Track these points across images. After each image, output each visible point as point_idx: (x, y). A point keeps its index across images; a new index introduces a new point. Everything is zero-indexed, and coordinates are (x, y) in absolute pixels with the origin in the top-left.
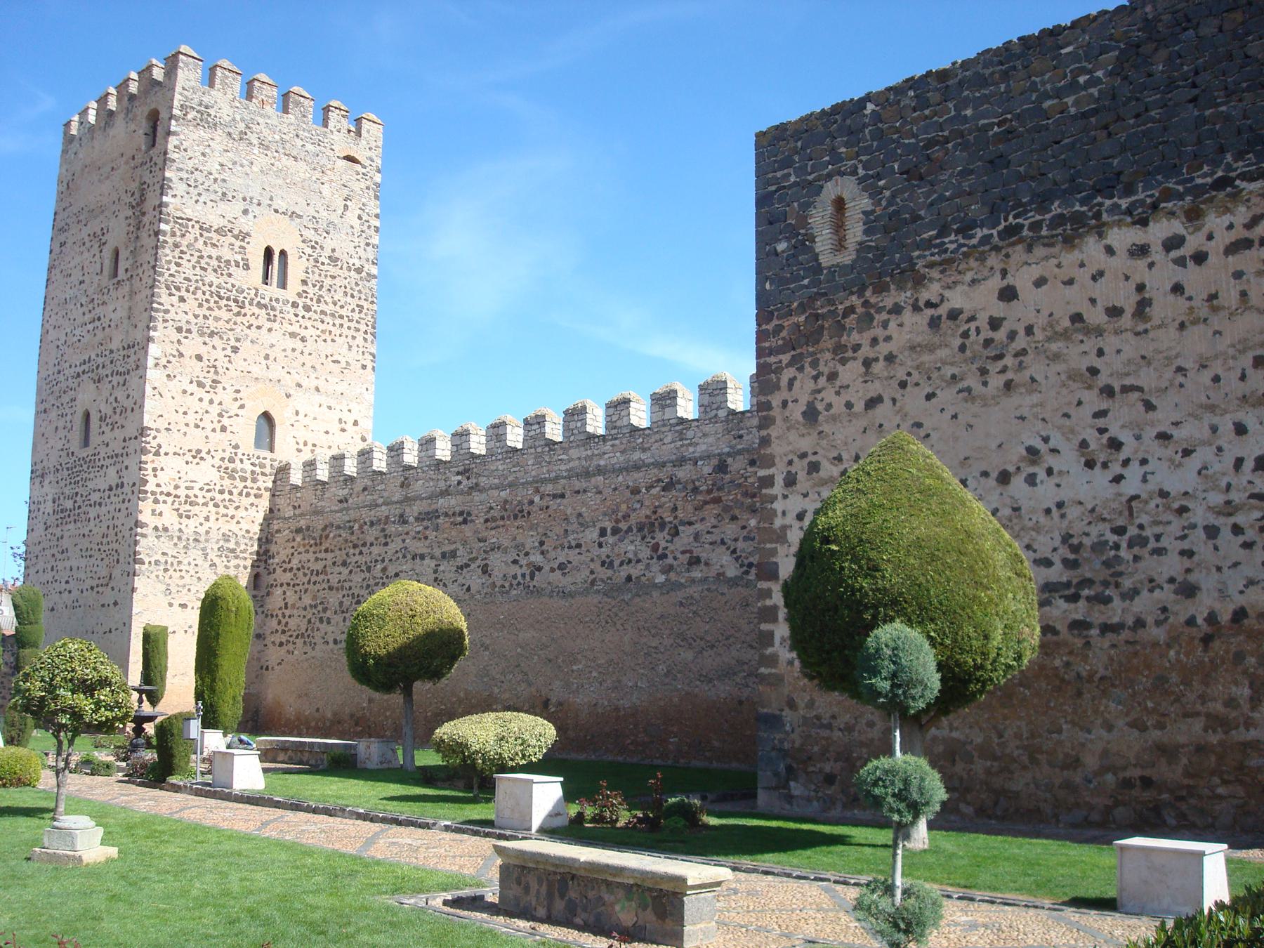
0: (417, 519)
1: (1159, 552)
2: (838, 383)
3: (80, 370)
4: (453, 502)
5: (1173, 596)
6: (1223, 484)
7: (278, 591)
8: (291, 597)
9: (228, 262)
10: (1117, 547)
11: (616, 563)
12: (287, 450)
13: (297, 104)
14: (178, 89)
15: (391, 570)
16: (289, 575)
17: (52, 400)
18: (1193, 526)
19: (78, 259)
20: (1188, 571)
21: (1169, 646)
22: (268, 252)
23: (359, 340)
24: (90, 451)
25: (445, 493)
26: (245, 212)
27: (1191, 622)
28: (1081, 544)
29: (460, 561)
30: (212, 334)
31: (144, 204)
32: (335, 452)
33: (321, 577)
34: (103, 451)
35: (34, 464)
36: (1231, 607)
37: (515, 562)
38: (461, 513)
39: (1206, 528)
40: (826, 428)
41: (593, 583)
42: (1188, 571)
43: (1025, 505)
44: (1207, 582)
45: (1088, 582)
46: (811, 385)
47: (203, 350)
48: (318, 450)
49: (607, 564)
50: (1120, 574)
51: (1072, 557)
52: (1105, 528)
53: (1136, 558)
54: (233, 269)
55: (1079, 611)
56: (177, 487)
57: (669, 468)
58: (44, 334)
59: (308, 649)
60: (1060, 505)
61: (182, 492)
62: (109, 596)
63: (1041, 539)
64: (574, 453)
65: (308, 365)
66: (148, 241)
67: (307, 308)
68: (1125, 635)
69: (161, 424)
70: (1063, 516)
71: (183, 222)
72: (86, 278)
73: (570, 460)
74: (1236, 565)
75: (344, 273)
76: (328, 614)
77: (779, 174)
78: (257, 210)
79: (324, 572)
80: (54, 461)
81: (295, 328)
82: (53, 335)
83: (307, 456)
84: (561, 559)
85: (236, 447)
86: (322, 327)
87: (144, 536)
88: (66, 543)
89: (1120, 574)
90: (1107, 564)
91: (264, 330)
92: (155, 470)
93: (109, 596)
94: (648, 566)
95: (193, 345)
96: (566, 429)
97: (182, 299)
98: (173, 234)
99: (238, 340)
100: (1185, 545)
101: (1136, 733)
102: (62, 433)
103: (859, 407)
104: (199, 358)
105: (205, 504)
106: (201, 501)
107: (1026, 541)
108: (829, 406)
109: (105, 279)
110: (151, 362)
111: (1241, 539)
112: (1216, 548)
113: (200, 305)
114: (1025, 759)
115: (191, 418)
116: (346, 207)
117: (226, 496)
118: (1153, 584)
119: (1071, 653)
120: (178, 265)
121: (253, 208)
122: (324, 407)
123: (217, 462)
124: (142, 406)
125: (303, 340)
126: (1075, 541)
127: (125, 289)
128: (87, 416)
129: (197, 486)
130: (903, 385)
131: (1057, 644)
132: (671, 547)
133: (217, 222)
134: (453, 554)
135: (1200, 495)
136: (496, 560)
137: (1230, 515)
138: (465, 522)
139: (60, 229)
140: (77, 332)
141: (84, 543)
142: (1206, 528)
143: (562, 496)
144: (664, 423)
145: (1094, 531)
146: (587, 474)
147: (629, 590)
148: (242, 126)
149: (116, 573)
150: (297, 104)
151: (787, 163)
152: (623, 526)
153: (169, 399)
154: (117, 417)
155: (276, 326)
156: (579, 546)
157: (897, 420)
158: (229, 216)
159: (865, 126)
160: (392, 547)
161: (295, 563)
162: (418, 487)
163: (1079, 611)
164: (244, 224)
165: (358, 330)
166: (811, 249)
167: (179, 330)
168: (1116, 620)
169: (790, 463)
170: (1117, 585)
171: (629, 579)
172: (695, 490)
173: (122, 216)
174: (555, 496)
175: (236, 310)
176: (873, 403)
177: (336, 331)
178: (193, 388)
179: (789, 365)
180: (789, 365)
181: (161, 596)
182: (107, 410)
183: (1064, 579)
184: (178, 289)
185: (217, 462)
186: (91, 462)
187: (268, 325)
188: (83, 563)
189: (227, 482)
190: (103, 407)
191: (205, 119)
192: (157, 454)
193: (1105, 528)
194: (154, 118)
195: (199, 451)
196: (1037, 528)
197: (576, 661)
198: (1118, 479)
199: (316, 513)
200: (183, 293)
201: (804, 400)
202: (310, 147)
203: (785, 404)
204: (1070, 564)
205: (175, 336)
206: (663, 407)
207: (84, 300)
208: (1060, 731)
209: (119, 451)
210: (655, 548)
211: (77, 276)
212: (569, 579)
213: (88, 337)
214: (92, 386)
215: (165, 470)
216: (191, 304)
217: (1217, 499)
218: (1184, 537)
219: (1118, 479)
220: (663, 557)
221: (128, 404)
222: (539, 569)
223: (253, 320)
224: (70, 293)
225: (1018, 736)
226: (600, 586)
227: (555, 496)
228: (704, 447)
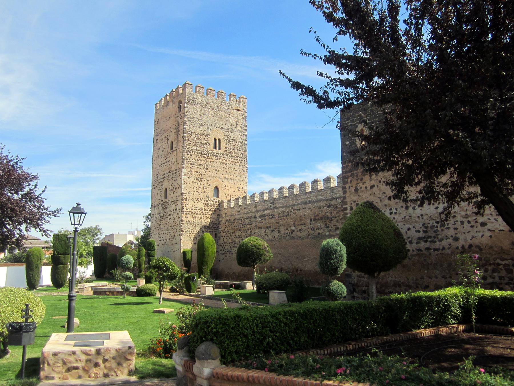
0: (260, 217)
1: (448, 228)
2: (363, 181)
3: (164, 176)
4: (269, 212)
5: (452, 241)
6: (465, 209)
7: (222, 238)
8: (225, 240)
9: (203, 143)
10: (437, 227)
11: (315, 229)
12: (223, 197)
13: (221, 95)
14: (187, 94)
15: (253, 232)
16: (225, 234)
17: (156, 185)
18: (457, 221)
19: (161, 144)
20: (456, 234)
21: (452, 255)
22: (215, 139)
23: (243, 163)
24: (167, 200)
25: (267, 209)
26: (208, 128)
27: (457, 248)
28: (428, 226)
29: (272, 229)
30: (200, 165)
31: (178, 128)
32: (236, 197)
33: (234, 234)
34: (171, 199)
35: (152, 204)
36: (468, 244)
37: (287, 229)
38: (272, 215)
39: (461, 222)
40: (361, 194)
41: (309, 235)
42: (456, 234)
43: (413, 215)
44: (461, 237)
45: (430, 237)
46: (356, 182)
47: (197, 170)
48: (232, 197)
49: (313, 229)
50: (438, 235)
51: (425, 230)
52: (434, 222)
53: (442, 230)
54: (205, 145)
55: (428, 245)
56: (192, 209)
57: (329, 201)
58: (153, 166)
59: (231, 255)
60: (422, 215)
61: (193, 211)
62: (174, 241)
63: (417, 225)
64: (302, 197)
65: (228, 172)
66: (181, 139)
67: (227, 155)
68: (440, 252)
69: (187, 192)
70: (423, 218)
71: (190, 133)
72: (164, 150)
73: (302, 199)
74: (469, 232)
75: (237, 144)
76: (236, 245)
77: (346, 122)
78: (211, 128)
79: (234, 233)
80: (157, 203)
81: (224, 161)
82: (155, 166)
83: (228, 198)
84: (300, 228)
85: (208, 197)
86: (231, 160)
87: (183, 224)
88: (162, 226)
89: (438, 235)
90: (435, 232)
91: (215, 163)
92: (185, 205)
93: (174, 241)
94: (324, 230)
95: (195, 168)
96: (300, 190)
97: (191, 155)
98: (188, 137)
99: (207, 166)
100: (455, 226)
101: (443, 279)
102: (159, 195)
103: (369, 188)
104: (197, 172)
105: (200, 214)
106: (199, 213)
107: (413, 225)
108: (361, 188)
109: (169, 151)
110: (183, 174)
111: (470, 225)
112: (464, 227)
113: (196, 157)
114: (415, 286)
115: (195, 189)
116: (237, 124)
117: (206, 211)
118: (447, 238)
119: (426, 257)
120: (189, 145)
121: (210, 127)
122: (233, 184)
123: (203, 201)
124: (181, 187)
125: (226, 164)
126: (426, 225)
127: (175, 153)
128: (166, 190)
129: (198, 209)
130: (380, 182)
131: (422, 254)
132: (330, 224)
133: (200, 132)
134: (270, 227)
135: (459, 212)
136: (282, 229)
137: (467, 218)
138: (273, 217)
139: (156, 135)
140: (162, 165)
141: (167, 226)
142: (461, 222)
143: (299, 210)
144: (327, 187)
145: (431, 222)
146: (306, 203)
147: (319, 237)
148: (205, 103)
149: (176, 235)
150: (221, 95)
151: (348, 119)
152: (317, 218)
153: (188, 185)
154: (174, 190)
155: (218, 161)
156: (305, 224)
157: (379, 192)
158: (203, 130)
159: (369, 108)
160: (253, 225)
161: (226, 230)
162: (260, 207)
163: (428, 245)
164: (208, 132)
165: (242, 160)
166: (355, 143)
167: (191, 164)
168: (437, 247)
169: (351, 204)
170: (438, 238)
171: (319, 234)
172: (337, 207)
173: (173, 132)
174: (297, 210)
175: (206, 157)
176: (372, 187)
177: (236, 161)
178: (195, 181)
179: (351, 176)
180: (351, 176)
181: (188, 241)
182: (171, 188)
183: (423, 236)
184: (190, 152)
185: (203, 201)
186: (167, 203)
187: (216, 161)
188: (167, 232)
189: (206, 207)
190: (170, 187)
191: (195, 102)
192: (186, 200)
193: (434, 222)
194: (180, 102)
195: (198, 199)
196: (416, 222)
197: (304, 258)
198: (437, 208)
199: (231, 215)
200: (191, 154)
201: (355, 186)
202: (225, 107)
203: (349, 187)
204: (425, 232)
205: (190, 166)
206: (327, 183)
207: (164, 156)
208: (424, 279)
209: (175, 200)
210: (326, 225)
211: (161, 149)
212: (302, 234)
213: (165, 167)
214: (167, 181)
215: (189, 205)
216: (194, 156)
217: (463, 213)
218: (455, 224)
219: (437, 208)
220: (328, 227)
221: (177, 186)
222: (294, 231)
223: (211, 160)
224: (160, 154)
225: (413, 280)
226: (311, 236)
227: (297, 210)
228: (338, 195)
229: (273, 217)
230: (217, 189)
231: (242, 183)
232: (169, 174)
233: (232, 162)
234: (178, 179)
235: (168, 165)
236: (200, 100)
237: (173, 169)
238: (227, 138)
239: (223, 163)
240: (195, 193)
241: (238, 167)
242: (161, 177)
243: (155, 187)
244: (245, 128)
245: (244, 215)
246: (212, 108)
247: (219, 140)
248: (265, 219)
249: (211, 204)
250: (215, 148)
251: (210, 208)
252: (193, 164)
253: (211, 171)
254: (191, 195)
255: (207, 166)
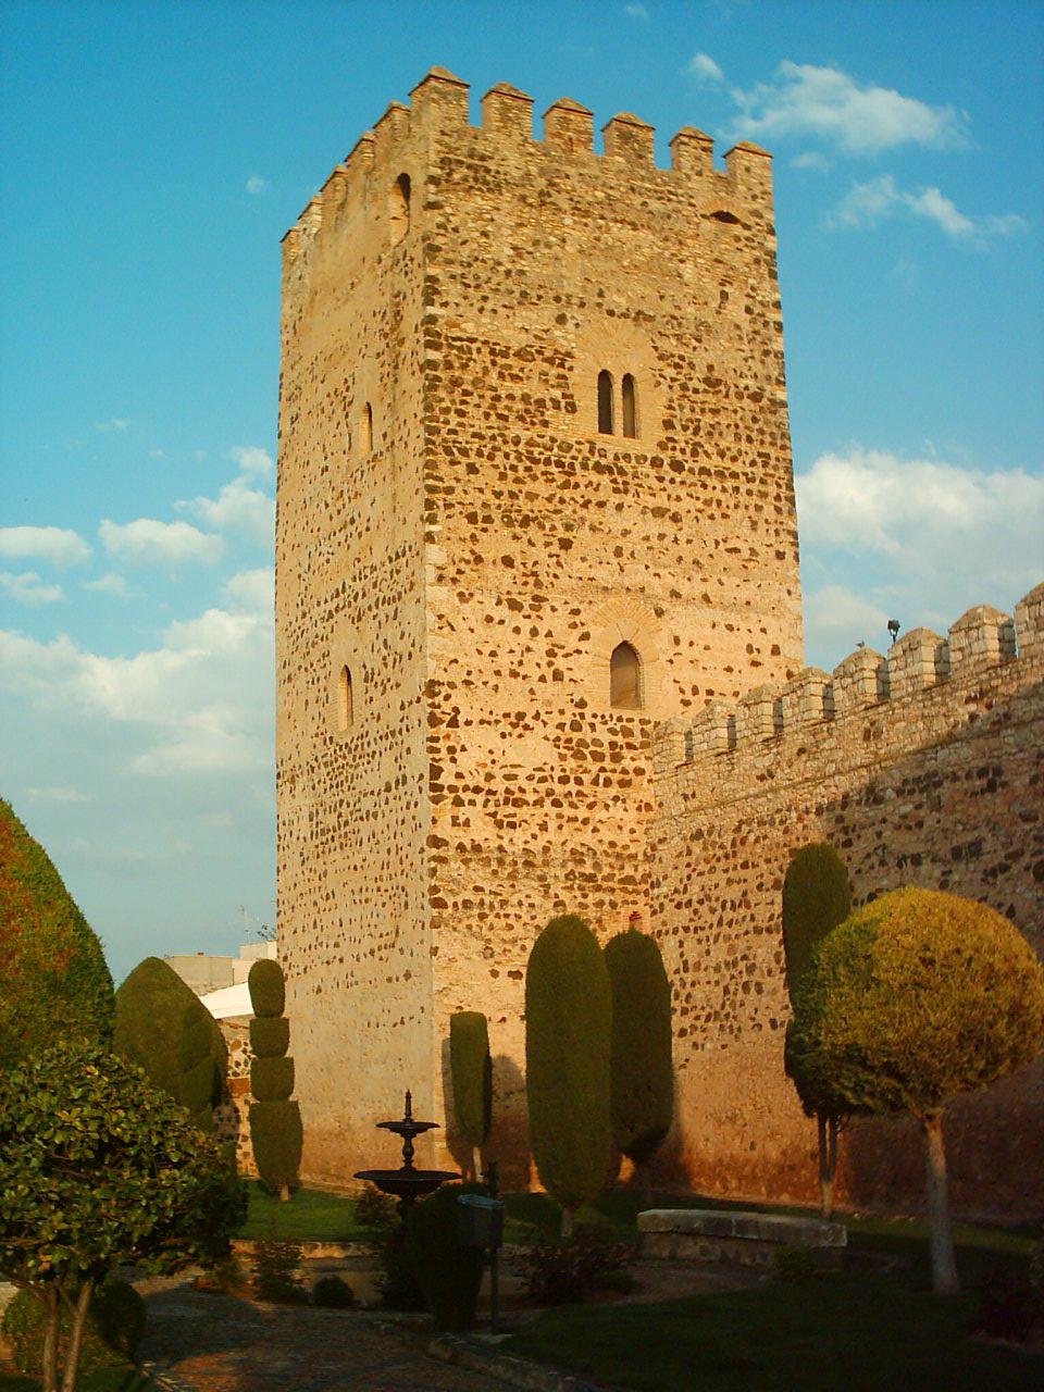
3: (331, 606)
9: (541, 403)
17: (297, 659)
22: (605, 377)
23: (769, 511)
26: (561, 319)
30: (525, 522)
33: (742, 911)
38: (982, 773)
47: (513, 549)
56: (489, 777)
59: (727, 1038)
61: (499, 785)
65: (688, 559)
67: (677, 466)
80: (306, 755)
81: (661, 501)
85: (582, 704)
88: (331, 883)
91: (610, 509)
92: (451, 750)
97: (472, 469)
98: (449, 366)
102: (314, 709)
104: (508, 562)
105: (539, 803)
106: (531, 797)
113: (503, 477)
115: (504, 661)
116: (724, 296)
117: (572, 787)
120: (461, 414)
123: (553, 732)
125: (676, 518)
133: (517, 341)
134: (975, 849)
141: (356, 881)
148: (541, 183)
155: (629, 499)
158: (536, 328)
161: (695, 892)
164: (564, 338)
167: (472, 518)
175: (560, 479)
178: (503, 612)
182: (374, 662)
184: (464, 452)
185: (553, 732)
187: (615, 499)
188: (357, 912)
189: (571, 763)
200: (473, 458)
202: (655, 205)
205: (467, 529)
209: (396, 726)
214: (351, 628)
216: (488, 476)
221: (403, 647)
223: (590, 494)
230: (625, 653)
231: (768, 621)
233: (708, 503)
234: (408, 608)
237: (379, 556)
238: (670, 372)
239: (659, 512)
240: (506, 681)
242: (318, 613)
243: (290, 669)
244: (773, 316)
245: (803, 791)
246: (580, 211)
247: (628, 380)
249: (596, 742)
250: (606, 426)
251: (594, 767)
252: (488, 519)
253: (589, 558)
254: (482, 691)
255: (568, 528)
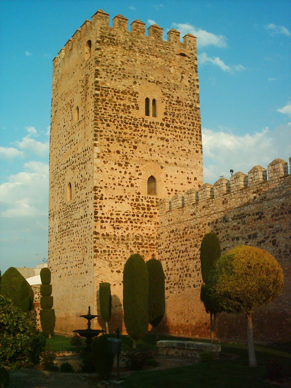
3: (66, 165)
8: (170, 265)
9: (128, 106)
17: (55, 181)
22: (147, 100)
23: (194, 139)
26: (135, 83)
29: (259, 239)
38: (257, 214)
47: (120, 148)
56: (112, 214)
59: (180, 290)
61: (115, 217)
67: (168, 126)
78: (140, 82)
80: (58, 208)
81: (163, 135)
85: (139, 193)
86: (175, 134)
88: (64, 245)
91: (148, 137)
92: (101, 206)
98: (102, 95)
102: (60, 195)
104: (118, 152)
105: (126, 222)
106: (124, 220)
113: (117, 128)
116: (182, 77)
117: (136, 217)
120: (105, 109)
123: (130, 202)
125: (167, 141)
129: (121, 213)
133: (122, 88)
134: (255, 236)
138: (260, 218)
141: (72, 244)
148: (130, 43)
149: (86, 257)
155: (154, 135)
158: (128, 85)
161: (171, 248)
164: (136, 88)
167: (108, 139)
175: (134, 129)
178: (116, 166)
184: (106, 120)
185: (130, 202)
187: (150, 135)
189: (136, 211)
192: (101, 199)
200: (109, 122)
202: (163, 51)
205: (106, 142)
209: (84, 199)
213: (69, 150)
214: (71, 172)
221: (87, 177)
223: (142, 133)
229: (260, 215)
230: (152, 179)
231: (193, 170)
232: (74, 159)
233: (176, 136)
234: (88, 165)
235: (73, 147)
236: (122, 38)
238: (166, 99)
239: (162, 139)
241: (187, 144)
242: (62, 167)
244: (196, 83)
247: (154, 101)
248: (244, 223)
249: (143, 204)
250: (147, 114)
251: (142, 212)
253: (142, 151)
254: (110, 189)
255: (136, 143)
